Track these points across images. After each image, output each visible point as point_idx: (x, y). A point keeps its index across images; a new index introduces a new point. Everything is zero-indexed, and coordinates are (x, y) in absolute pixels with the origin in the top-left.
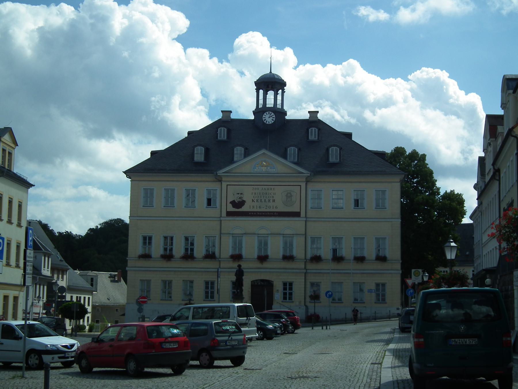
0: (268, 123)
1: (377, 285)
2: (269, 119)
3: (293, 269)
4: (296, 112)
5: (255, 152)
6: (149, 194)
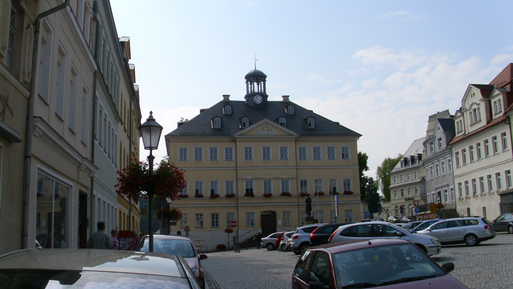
2: (258, 100)
4: (274, 96)
5: (256, 122)
6: (183, 152)
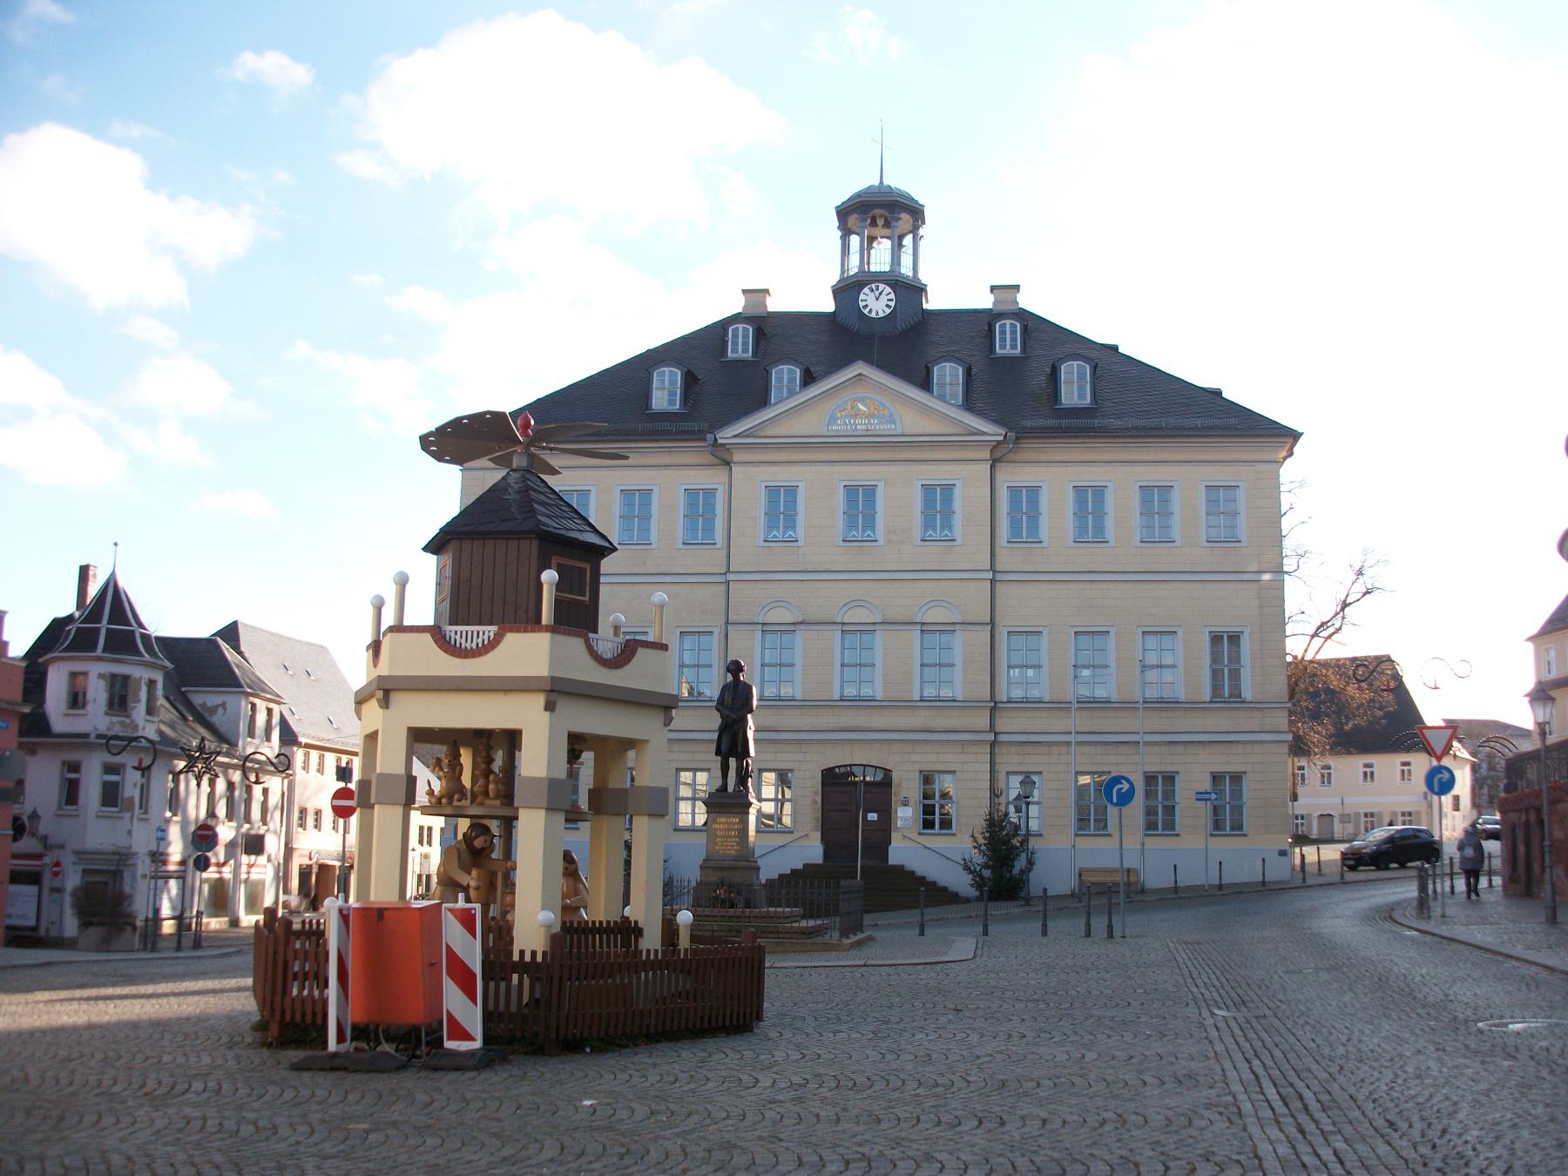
0: (873, 315)
1: (1217, 778)
2: (877, 303)
3: (213, 991)
4: (953, 282)
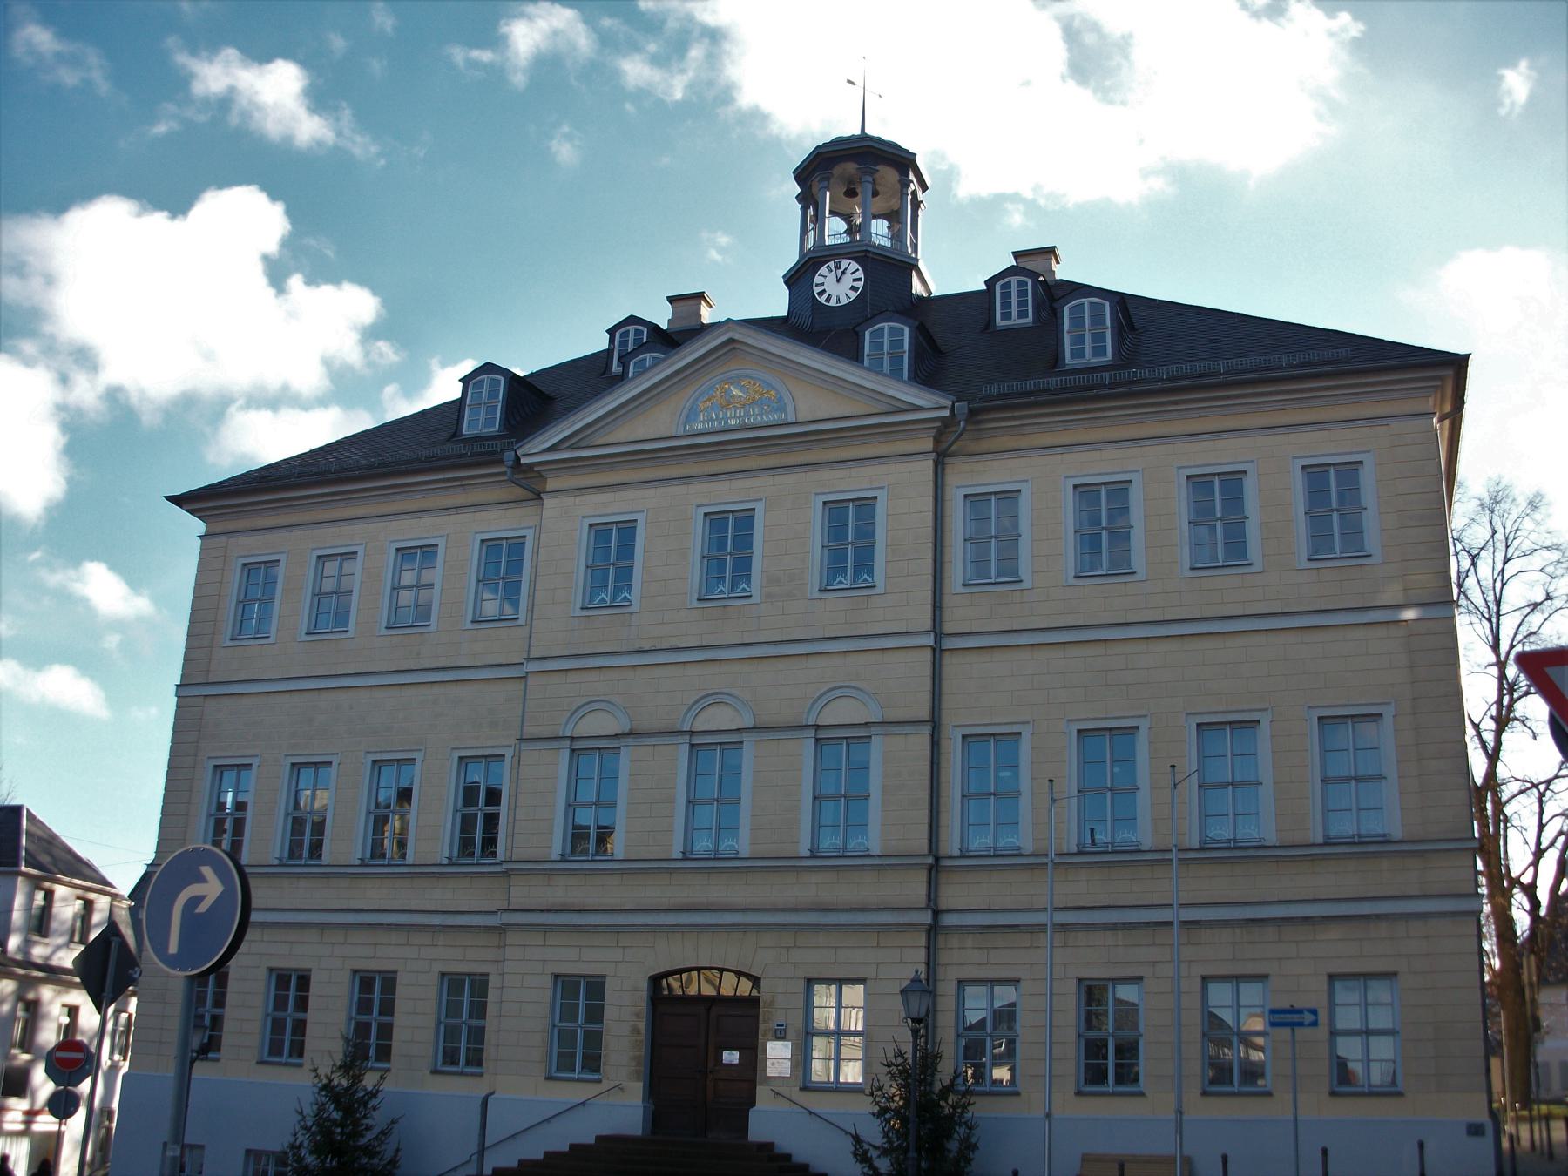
0: (833, 303)
